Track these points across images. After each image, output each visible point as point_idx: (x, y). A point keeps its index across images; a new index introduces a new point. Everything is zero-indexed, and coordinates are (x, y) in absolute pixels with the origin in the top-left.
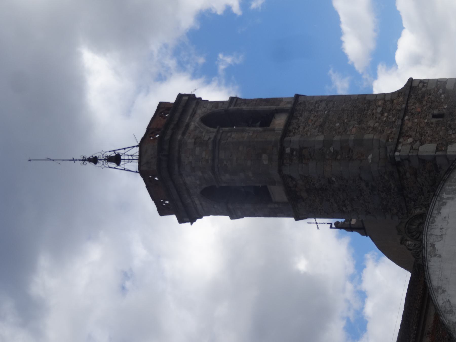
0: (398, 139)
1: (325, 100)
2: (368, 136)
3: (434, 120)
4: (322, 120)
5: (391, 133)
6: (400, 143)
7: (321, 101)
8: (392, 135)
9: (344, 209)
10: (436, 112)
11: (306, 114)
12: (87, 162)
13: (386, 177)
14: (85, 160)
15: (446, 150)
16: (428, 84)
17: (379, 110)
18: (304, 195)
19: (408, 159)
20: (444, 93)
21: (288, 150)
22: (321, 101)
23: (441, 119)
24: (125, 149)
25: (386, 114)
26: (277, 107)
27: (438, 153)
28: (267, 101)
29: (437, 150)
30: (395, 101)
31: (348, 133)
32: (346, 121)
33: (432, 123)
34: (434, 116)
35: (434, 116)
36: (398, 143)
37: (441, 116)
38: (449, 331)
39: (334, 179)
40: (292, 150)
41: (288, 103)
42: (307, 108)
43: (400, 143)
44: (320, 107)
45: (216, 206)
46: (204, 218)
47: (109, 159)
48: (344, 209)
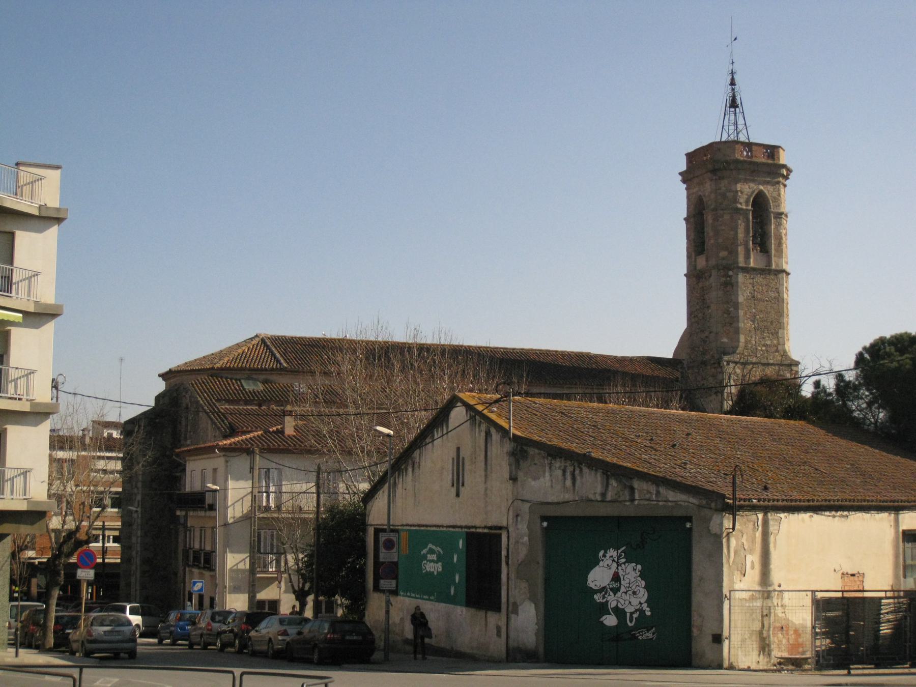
2: (742, 338)
4: (759, 297)
9: (693, 316)
11: (764, 282)
13: (711, 353)
16: (50, 456)
17: (769, 342)
18: (700, 285)
21: (730, 273)
25: (764, 348)
26: (491, 531)
28: (780, 244)
30: (777, 354)
31: (746, 321)
32: (758, 317)
36: (736, 363)
38: (63, 649)
40: (730, 277)
41: (777, 265)
42: (772, 281)
46: (686, 191)
48: (693, 316)
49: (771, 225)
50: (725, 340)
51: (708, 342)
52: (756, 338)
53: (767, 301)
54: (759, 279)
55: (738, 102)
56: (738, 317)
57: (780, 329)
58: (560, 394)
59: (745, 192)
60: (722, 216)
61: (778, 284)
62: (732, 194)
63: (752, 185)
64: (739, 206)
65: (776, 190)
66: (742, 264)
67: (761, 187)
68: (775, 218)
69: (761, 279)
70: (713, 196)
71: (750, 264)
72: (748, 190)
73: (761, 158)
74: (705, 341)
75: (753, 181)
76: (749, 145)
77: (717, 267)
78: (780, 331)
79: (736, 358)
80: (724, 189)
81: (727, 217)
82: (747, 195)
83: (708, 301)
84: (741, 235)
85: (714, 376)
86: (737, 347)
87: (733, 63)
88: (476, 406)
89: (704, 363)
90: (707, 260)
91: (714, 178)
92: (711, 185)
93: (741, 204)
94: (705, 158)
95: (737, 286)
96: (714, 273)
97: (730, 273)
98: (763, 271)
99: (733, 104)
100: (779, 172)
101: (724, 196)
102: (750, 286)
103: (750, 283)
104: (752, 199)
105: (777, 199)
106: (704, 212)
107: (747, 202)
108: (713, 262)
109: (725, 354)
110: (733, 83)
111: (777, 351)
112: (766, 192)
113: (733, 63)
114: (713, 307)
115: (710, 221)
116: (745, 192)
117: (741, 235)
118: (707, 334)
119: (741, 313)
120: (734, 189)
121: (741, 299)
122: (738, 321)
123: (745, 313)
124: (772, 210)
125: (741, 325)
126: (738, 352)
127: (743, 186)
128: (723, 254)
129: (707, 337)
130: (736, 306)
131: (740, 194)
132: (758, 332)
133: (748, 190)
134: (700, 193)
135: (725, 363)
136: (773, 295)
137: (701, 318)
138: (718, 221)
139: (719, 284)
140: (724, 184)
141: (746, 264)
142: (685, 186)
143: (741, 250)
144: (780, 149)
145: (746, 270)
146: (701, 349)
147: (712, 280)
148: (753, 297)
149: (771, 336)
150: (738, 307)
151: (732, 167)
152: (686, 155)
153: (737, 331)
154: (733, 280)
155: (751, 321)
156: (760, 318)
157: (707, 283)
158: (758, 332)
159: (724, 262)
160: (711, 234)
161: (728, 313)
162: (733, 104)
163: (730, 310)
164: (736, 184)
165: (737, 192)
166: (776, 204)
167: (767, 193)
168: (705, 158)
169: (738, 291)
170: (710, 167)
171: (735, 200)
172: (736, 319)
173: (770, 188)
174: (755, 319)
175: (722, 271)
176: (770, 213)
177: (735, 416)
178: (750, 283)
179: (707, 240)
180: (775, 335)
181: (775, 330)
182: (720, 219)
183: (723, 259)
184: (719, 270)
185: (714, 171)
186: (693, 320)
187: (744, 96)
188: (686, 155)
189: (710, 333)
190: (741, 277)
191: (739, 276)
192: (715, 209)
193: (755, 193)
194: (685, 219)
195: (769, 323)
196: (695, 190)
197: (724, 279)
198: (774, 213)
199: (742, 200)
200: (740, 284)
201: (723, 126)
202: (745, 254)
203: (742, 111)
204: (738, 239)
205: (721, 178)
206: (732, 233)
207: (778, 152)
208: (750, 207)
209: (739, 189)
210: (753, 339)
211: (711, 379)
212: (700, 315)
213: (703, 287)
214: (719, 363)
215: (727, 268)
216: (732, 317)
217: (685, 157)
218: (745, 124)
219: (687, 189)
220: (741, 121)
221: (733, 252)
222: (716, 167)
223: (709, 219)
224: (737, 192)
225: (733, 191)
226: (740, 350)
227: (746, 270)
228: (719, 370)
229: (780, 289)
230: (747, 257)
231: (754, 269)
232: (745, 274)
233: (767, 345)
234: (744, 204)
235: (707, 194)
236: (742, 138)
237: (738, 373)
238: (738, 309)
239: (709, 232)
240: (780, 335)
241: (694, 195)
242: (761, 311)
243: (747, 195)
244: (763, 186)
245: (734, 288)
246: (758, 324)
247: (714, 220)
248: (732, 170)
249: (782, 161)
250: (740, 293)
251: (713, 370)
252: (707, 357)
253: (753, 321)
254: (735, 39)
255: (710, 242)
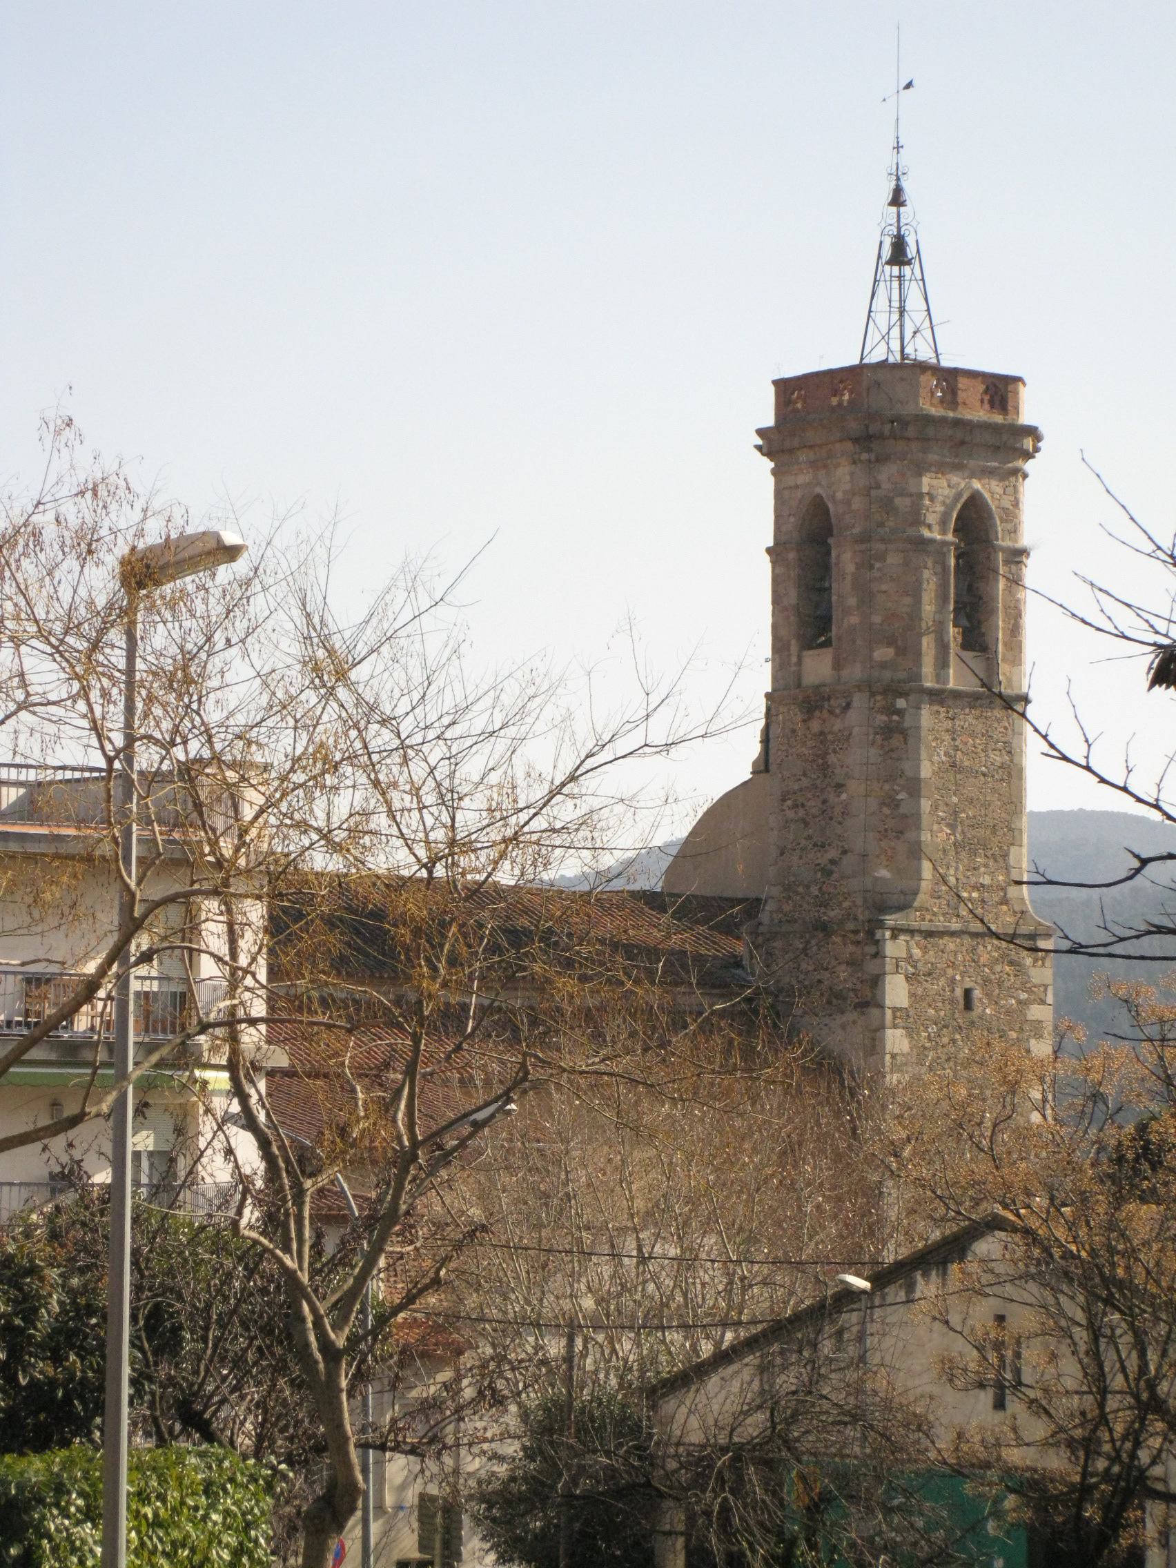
0: (920, 931)
1: (1012, 761)
3: (959, 992)
4: (966, 763)
5: (934, 914)
6: (912, 936)
7: (1009, 752)
8: (928, 917)
10: (977, 993)
11: (980, 728)
12: (893, 183)
13: (846, 904)
14: (898, 179)
15: (895, 1026)
17: (986, 880)
18: (815, 726)
19: (879, 955)
20: (1020, 1002)
21: (901, 703)
22: (1009, 752)
23: (961, 1006)
24: (923, 279)
25: (975, 895)
27: (889, 1013)
28: (1015, 630)
29: (895, 1010)
30: (1005, 908)
31: (936, 827)
32: (963, 815)
33: (953, 991)
34: (968, 993)
35: (968, 993)
37: (968, 1005)
39: (844, 796)
40: (900, 712)
41: (1009, 680)
42: (996, 725)
43: (912, 936)
44: (997, 753)
45: (792, 519)
46: (772, 479)
47: (899, 245)
48: (789, 803)
49: (997, 581)
50: (884, 873)
51: (835, 876)
52: (957, 869)
53: (984, 775)
54: (968, 719)
55: (911, 251)
56: (918, 815)
57: (1013, 844)
58: (35, 854)
59: (941, 498)
60: (882, 557)
61: (1010, 732)
62: (908, 501)
63: (955, 479)
64: (926, 533)
65: (1010, 490)
66: (929, 684)
67: (977, 485)
68: (1007, 562)
69: (970, 719)
70: (857, 503)
71: (946, 681)
72: (947, 491)
73: (979, 413)
74: (828, 873)
75: (958, 467)
76: (951, 377)
77: (869, 687)
78: (1013, 850)
79: (911, 919)
80: (886, 486)
81: (893, 559)
82: (944, 503)
83: (837, 771)
84: (928, 608)
85: (853, 963)
86: (916, 893)
87: (898, 147)
88: (1084, 1322)
89: (824, 928)
90: (837, 665)
91: (865, 456)
92: (852, 474)
93: (929, 527)
94: (835, 401)
95: (919, 739)
96: (859, 700)
97: (901, 703)
98: (978, 699)
99: (899, 254)
100: (1018, 445)
101: (887, 505)
102: (947, 737)
103: (947, 731)
104: (955, 515)
105: (1012, 514)
106: (831, 541)
107: (943, 523)
108: (855, 672)
109: (884, 908)
110: (897, 199)
111: (1004, 901)
112: (987, 495)
113: (898, 147)
114: (855, 787)
115: (850, 568)
116: (941, 498)
117: (928, 608)
118: (832, 853)
119: (925, 805)
120: (913, 490)
121: (926, 771)
122: (918, 827)
123: (935, 807)
124: (1000, 542)
125: (926, 836)
126: (916, 904)
127: (935, 482)
128: (884, 653)
129: (832, 862)
130: (914, 787)
131: (927, 502)
132: (963, 855)
133: (947, 491)
134: (818, 490)
135: (888, 934)
136: (997, 758)
137: (814, 811)
138: (871, 567)
139: (871, 730)
140: (887, 473)
141: (938, 682)
142: (772, 465)
143: (928, 644)
144: (1020, 384)
145: (938, 697)
146: (814, 890)
147: (853, 716)
148: (953, 765)
149: (991, 863)
150: (919, 791)
151: (911, 431)
152: (776, 383)
153: (916, 852)
154: (907, 723)
155: (948, 825)
156: (968, 817)
157: (838, 725)
158: (963, 855)
159: (887, 675)
160: (852, 601)
161: (896, 805)
162: (899, 254)
163: (900, 797)
164: (920, 475)
165: (921, 496)
166: (1009, 526)
167: (989, 501)
168: (835, 401)
169: (919, 748)
170: (854, 426)
171: (917, 519)
172: (911, 821)
173: (996, 486)
174: (955, 820)
175: (879, 698)
176: (995, 549)
177: (951, 671)
178: (947, 731)
179: (836, 614)
180: (1000, 860)
181: (1000, 848)
182: (878, 565)
183: (883, 665)
184: (873, 694)
185: (865, 440)
186: (790, 814)
187: (920, 237)
188: (776, 383)
189: (845, 852)
190: (927, 717)
191: (923, 712)
192: (865, 538)
193: (963, 500)
194: (769, 551)
195: (988, 832)
196: (802, 479)
197: (885, 718)
198: (1003, 549)
199: (932, 518)
200: (924, 733)
201: (870, 311)
202: (936, 659)
203: (919, 277)
204: (921, 619)
205: (881, 460)
206: (908, 600)
207: (1016, 393)
208: (950, 537)
209: (925, 489)
210: (952, 871)
211: (843, 973)
212: (812, 803)
213: (822, 733)
214: (871, 933)
215: (894, 690)
216: (905, 816)
217: (772, 389)
218: (928, 310)
219: (775, 472)
220: (914, 301)
221: (908, 650)
222: (872, 430)
223: (845, 559)
224: (921, 496)
225: (911, 495)
226: (921, 899)
227: (938, 697)
228: (871, 949)
229: (1014, 745)
230: (942, 663)
231: (956, 695)
232: (935, 708)
233: (983, 886)
234: (936, 528)
235: (839, 495)
236: (921, 351)
237: (916, 957)
238: (919, 797)
239: (843, 592)
240: (1012, 860)
241: (799, 494)
242: (971, 801)
243: (944, 503)
244: (980, 479)
245: (911, 741)
246: (963, 832)
247: (859, 566)
248: (909, 439)
249: (1027, 417)
250: (924, 754)
251: (851, 948)
252: (834, 913)
253: (952, 827)
254: (909, 86)
255: (847, 619)
